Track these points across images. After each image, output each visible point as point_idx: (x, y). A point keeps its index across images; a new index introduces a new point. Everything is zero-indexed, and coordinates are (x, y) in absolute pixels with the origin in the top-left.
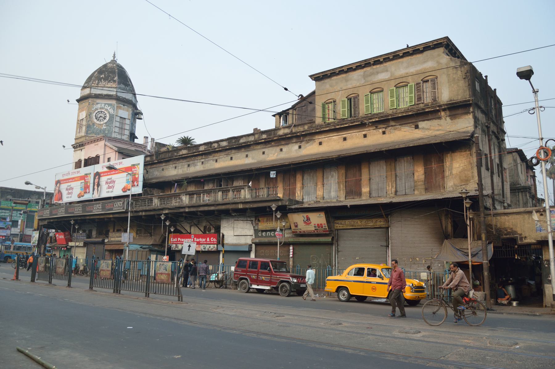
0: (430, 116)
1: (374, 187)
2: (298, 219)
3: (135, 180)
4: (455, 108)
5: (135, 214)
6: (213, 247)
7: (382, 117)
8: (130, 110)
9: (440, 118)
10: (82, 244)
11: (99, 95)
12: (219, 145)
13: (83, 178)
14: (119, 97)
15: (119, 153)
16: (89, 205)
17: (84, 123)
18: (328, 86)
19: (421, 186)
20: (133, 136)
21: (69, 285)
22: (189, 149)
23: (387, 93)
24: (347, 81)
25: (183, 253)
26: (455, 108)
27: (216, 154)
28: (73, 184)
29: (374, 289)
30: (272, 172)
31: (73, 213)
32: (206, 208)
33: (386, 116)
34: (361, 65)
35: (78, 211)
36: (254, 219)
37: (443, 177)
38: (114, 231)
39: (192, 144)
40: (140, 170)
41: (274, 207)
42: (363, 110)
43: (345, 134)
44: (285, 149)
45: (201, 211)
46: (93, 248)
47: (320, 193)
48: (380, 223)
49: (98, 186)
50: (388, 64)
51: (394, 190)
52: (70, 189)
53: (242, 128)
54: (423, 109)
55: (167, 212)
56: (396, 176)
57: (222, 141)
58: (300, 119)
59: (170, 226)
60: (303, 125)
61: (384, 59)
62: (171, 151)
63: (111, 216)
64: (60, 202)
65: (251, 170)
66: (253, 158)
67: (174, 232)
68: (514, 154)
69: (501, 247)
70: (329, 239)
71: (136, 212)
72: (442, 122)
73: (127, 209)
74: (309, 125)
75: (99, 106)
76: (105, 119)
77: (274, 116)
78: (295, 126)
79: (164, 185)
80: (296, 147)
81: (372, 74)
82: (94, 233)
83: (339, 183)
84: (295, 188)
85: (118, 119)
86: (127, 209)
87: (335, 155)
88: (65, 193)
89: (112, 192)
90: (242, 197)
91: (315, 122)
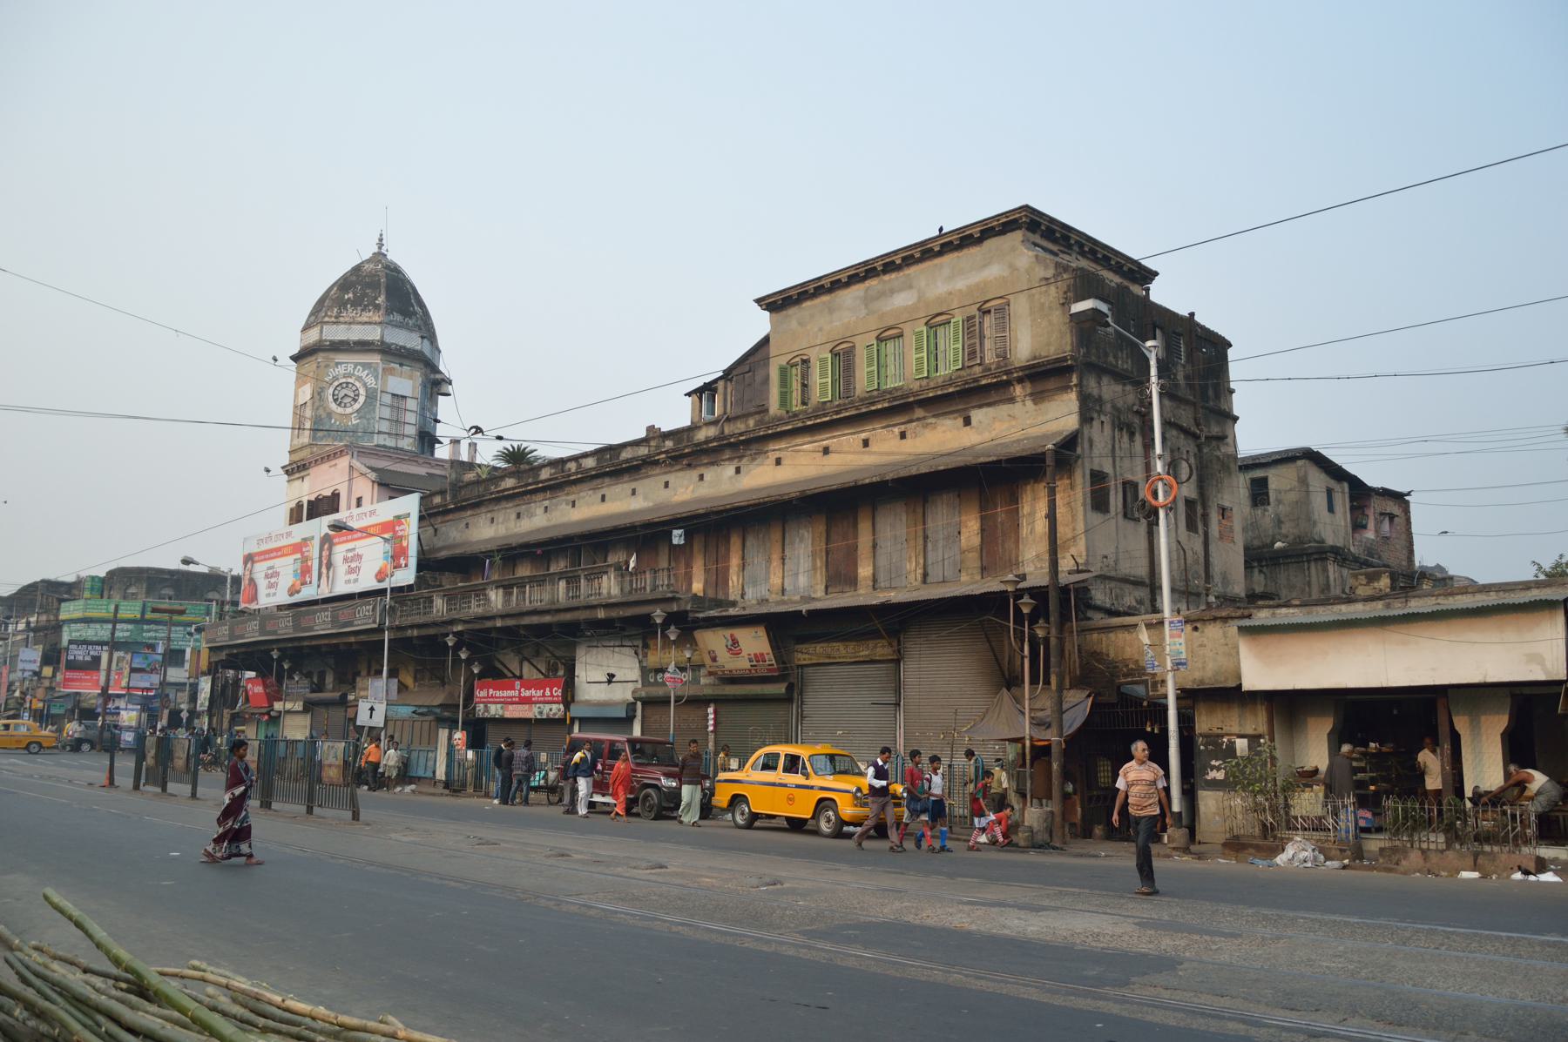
0: (994, 397)
1: (882, 561)
2: (714, 641)
3: (397, 555)
4: (1043, 376)
5: (400, 635)
6: (556, 710)
7: (895, 399)
8: (418, 376)
9: (1012, 400)
10: (299, 706)
11: (342, 342)
12: (579, 466)
13: (297, 548)
14: (389, 345)
15: (380, 484)
16: (308, 613)
17: (308, 413)
18: (794, 324)
19: (973, 560)
20: (427, 439)
21: (194, 795)
22: (525, 475)
23: (910, 340)
24: (831, 311)
25: (359, 723)
26: (1043, 376)
27: (574, 488)
28: (278, 563)
29: (791, 800)
30: (676, 532)
31: (275, 633)
32: (535, 620)
33: (902, 397)
34: (857, 275)
35: (285, 628)
36: (639, 643)
37: (1017, 541)
38: (369, 674)
39: (529, 463)
40: (411, 528)
41: (658, 615)
42: (863, 380)
43: (827, 440)
44: (710, 474)
45: (527, 627)
46: (323, 713)
47: (776, 580)
48: (882, 650)
49: (328, 569)
50: (912, 271)
51: (920, 571)
52: (272, 574)
53: (623, 427)
54: (976, 380)
55: (460, 628)
56: (926, 538)
57: (585, 455)
58: (742, 406)
59: (469, 662)
60: (746, 416)
61: (904, 259)
62: (484, 481)
63: (352, 639)
64: (253, 606)
65: (632, 528)
66: (645, 498)
67: (481, 676)
68: (1300, 463)
69: (1113, 705)
70: (779, 689)
71: (399, 628)
72: (1016, 409)
73: (382, 624)
74: (757, 417)
75: (341, 370)
76: (355, 400)
77: (689, 394)
78: (728, 420)
79: (467, 565)
80: (730, 470)
81: (882, 294)
82: (329, 679)
83: (814, 555)
84: (727, 569)
85: (387, 399)
86: (382, 624)
87: (793, 492)
88: (262, 584)
89: (356, 581)
90: (604, 591)
91: (767, 411)
